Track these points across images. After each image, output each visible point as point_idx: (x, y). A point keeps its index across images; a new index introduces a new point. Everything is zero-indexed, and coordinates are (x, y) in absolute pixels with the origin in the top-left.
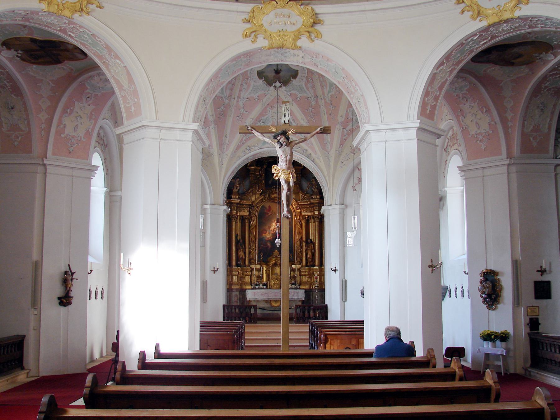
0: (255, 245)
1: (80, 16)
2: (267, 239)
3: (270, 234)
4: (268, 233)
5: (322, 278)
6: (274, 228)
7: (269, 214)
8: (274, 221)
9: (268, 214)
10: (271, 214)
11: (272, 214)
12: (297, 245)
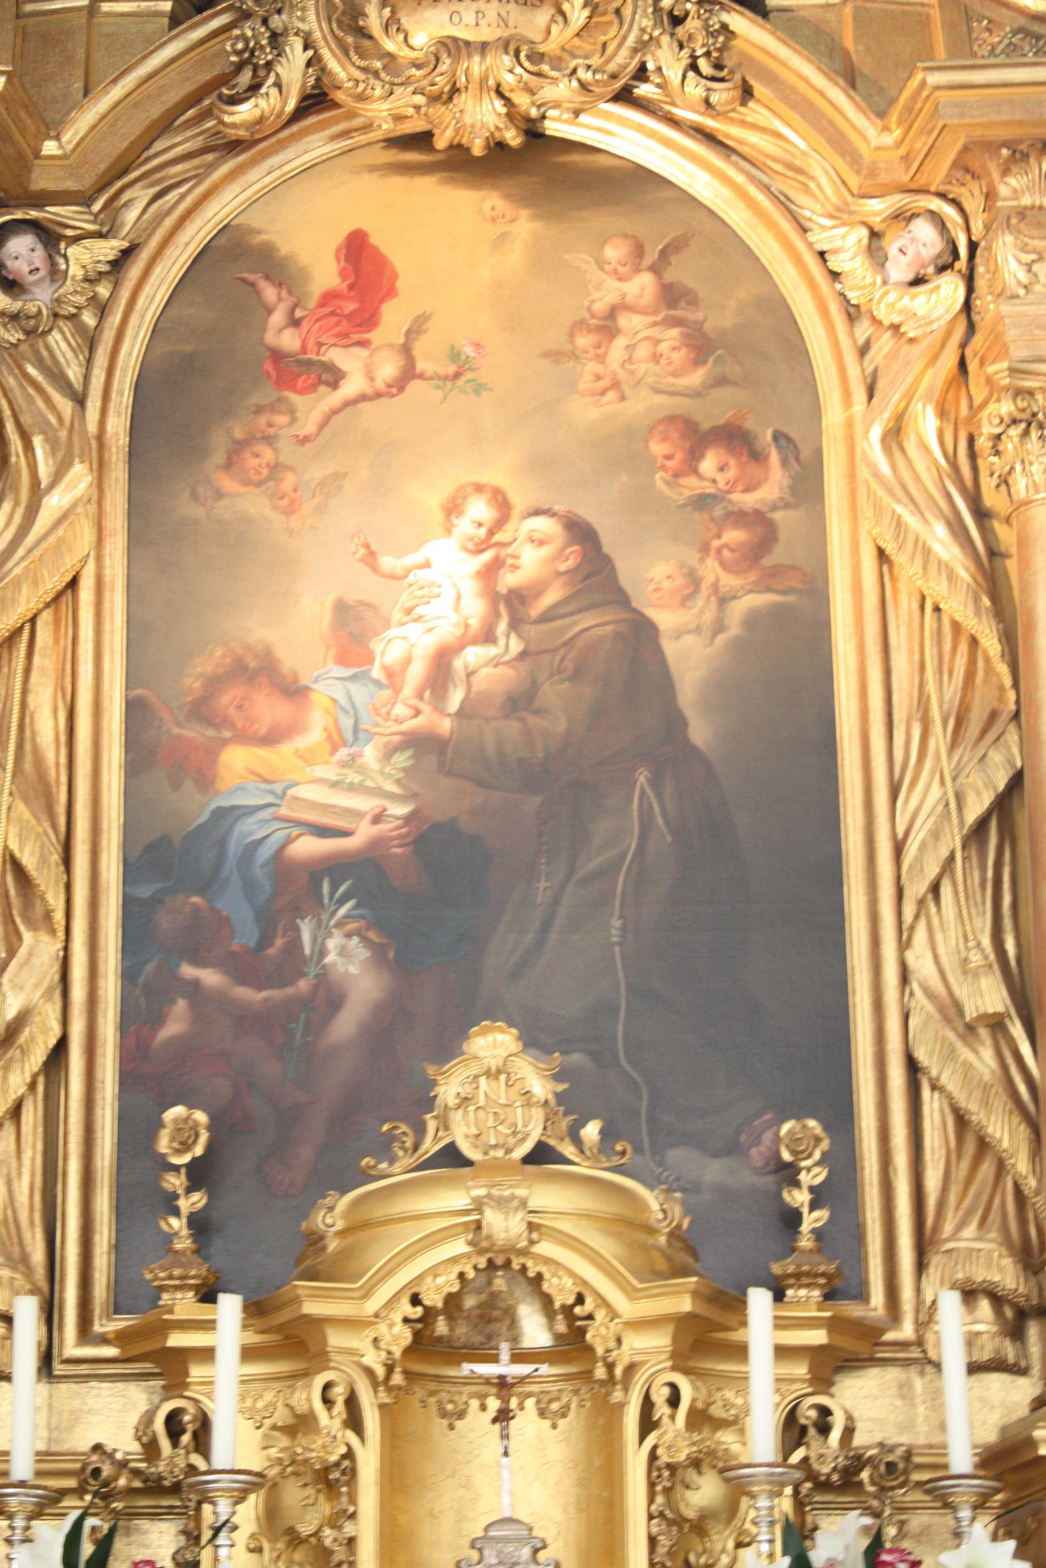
0: (49, 948)
1: (458, 1094)
2: (307, 847)
3: (370, 754)
4: (314, 736)
5: (313, 805)
6: (446, 631)
7: (350, 387)
8: (453, 508)
9: (334, 377)
10: (388, 369)
11: (408, 374)
12: (921, 961)
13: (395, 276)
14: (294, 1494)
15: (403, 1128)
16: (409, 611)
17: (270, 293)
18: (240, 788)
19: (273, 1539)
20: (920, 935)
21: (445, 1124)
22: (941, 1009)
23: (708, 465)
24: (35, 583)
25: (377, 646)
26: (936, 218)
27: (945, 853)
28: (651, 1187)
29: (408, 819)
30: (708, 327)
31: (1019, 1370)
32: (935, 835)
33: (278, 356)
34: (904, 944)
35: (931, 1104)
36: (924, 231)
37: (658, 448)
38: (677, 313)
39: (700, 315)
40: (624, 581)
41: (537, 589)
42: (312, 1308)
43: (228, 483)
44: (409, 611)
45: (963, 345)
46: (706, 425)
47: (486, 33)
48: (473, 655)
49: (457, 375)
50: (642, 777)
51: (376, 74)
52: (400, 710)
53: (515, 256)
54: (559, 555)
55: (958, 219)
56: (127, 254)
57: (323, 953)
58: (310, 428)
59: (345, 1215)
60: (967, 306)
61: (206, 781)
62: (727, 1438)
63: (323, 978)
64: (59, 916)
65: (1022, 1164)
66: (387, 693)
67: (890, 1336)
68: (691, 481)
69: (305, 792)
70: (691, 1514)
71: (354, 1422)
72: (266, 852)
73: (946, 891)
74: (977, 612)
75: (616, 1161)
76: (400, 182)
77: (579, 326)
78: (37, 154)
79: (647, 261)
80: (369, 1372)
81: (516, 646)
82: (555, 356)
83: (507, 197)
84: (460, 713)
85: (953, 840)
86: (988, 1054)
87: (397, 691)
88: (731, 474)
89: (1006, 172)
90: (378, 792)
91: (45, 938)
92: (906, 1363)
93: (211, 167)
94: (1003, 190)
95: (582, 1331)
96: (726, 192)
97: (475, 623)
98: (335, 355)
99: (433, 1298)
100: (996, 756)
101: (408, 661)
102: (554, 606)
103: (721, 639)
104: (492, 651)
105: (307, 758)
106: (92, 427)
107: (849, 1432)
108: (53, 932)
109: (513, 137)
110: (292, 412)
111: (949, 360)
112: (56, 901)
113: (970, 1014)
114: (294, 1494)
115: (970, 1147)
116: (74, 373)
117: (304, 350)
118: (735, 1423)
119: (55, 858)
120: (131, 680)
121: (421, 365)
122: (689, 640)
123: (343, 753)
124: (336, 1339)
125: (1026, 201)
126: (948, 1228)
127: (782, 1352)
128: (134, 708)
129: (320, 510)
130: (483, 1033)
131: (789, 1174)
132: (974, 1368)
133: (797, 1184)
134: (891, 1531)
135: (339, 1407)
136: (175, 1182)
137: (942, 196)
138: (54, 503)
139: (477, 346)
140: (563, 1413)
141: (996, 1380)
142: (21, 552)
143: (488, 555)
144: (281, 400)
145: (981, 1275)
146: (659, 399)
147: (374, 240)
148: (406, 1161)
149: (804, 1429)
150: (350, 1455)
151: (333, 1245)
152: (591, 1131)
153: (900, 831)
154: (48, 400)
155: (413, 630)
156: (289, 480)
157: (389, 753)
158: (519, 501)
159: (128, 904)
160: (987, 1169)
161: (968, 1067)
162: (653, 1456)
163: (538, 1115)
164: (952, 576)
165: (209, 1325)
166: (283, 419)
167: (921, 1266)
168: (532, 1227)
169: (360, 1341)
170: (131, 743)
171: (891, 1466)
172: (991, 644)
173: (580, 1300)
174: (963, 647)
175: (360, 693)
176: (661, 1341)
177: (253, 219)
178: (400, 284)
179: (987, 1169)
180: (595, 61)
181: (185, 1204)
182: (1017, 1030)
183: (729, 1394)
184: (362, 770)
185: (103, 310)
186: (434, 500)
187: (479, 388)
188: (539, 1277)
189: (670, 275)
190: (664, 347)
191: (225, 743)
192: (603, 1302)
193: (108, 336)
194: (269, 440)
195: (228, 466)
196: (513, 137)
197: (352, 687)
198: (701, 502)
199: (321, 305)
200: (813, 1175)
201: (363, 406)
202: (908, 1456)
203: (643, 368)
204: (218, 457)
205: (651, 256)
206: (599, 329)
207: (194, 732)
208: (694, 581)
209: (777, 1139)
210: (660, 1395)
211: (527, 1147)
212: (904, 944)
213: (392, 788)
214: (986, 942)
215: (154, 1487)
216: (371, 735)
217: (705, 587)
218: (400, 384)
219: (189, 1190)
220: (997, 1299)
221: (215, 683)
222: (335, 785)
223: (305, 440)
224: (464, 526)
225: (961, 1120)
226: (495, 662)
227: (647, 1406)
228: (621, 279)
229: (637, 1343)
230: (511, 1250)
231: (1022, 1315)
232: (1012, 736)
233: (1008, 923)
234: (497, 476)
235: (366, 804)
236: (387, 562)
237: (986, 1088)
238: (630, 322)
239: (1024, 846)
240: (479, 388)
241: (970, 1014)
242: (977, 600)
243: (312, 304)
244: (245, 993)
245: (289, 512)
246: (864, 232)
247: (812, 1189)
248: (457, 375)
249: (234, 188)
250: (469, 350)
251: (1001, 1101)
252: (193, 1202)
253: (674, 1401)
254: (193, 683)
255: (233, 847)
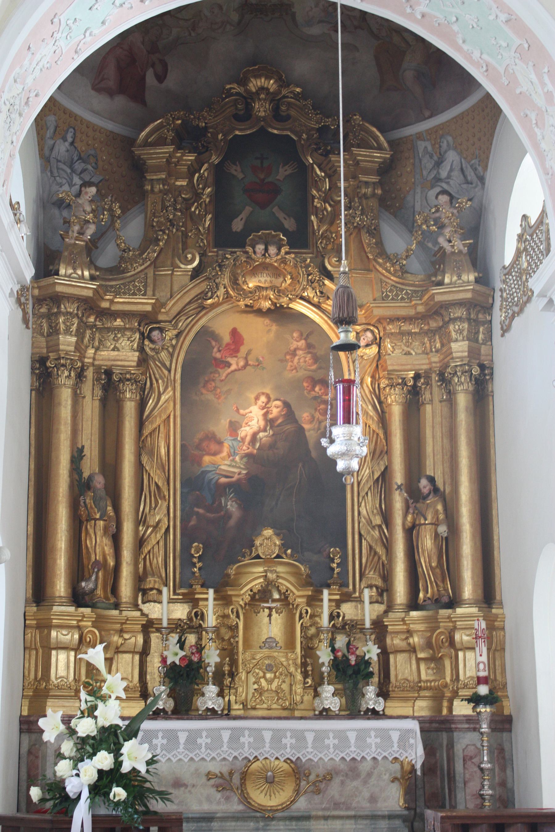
2: (223, 480)
3: (237, 458)
4: (224, 454)
5: (224, 470)
6: (255, 428)
7: (233, 367)
8: (257, 398)
9: (229, 365)
10: (242, 363)
11: (246, 365)
12: (364, 512)
13: (243, 339)
14: (223, 630)
15: (247, 550)
16: (247, 424)
17: (214, 343)
18: (208, 466)
19: (219, 640)
20: (363, 504)
21: (256, 549)
22: (367, 522)
23: (317, 389)
24: (160, 417)
25: (239, 432)
26: (372, 332)
27: (369, 486)
28: (302, 564)
29: (246, 474)
30: (318, 354)
31: (382, 603)
32: (367, 481)
33: (215, 359)
34: (359, 506)
35: (364, 543)
36: (369, 334)
37: (305, 384)
38: (311, 350)
39: (316, 351)
40: (297, 417)
41: (276, 419)
42: (230, 593)
43: (204, 391)
44: (247, 424)
45: (378, 361)
46: (317, 379)
47: (267, 285)
48: (261, 434)
49: (258, 365)
50: (300, 465)
51: (241, 295)
52: (244, 448)
53: (272, 335)
54: (282, 411)
55: (377, 331)
56: (179, 333)
57: (227, 506)
58: (223, 378)
59: (235, 570)
60: (379, 352)
61: (200, 464)
62: (317, 619)
63: (227, 511)
64: (167, 497)
65: (384, 558)
66: (241, 444)
67: (353, 596)
68: (313, 393)
69: (223, 467)
70: (309, 636)
71: (238, 616)
72: (214, 481)
73: (369, 494)
74: (378, 428)
75: (294, 558)
76: (244, 315)
77: (287, 353)
78: (160, 311)
79: (303, 337)
80: (241, 606)
81: (271, 433)
82: (281, 361)
83: (270, 320)
84: (259, 449)
85: (371, 483)
86: (377, 532)
87: (244, 443)
88: (322, 391)
89: (388, 324)
90: (239, 467)
91: (164, 502)
92: (357, 601)
93: (200, 312)
94: (388, 328)
95: (287, 597)
96: (323, 321)
97: (262, 427)
98: (229, 359)
99: (255, 590)
100: (382, 463)
101: (246, 436)
102: (281, 423)
103: (319, 432)
104: (266, 434)
105: (223, 459)
106: (172, 378)
107: (344, 617)
108: (165, 500)
109: (273, 308)
110: (219, 373)
111: (374, 365)
112: (166, 493)
113: (374, 524)
114: (223, 630)
115: (373, 554)
116: (168, 364)
117: (222, 358)
118: (319, 616)
119: (166, 483)
120: (182, 439)
121: (250, 362)
122: (312, 432)
123: (231, 458)
124: (234, 599)
125: (393, 331)
126: (367, 572)
127: (330, 600)
128: (182, 446)
129: (225, 398)
130: (266, 530)
131: (332, 560)
132: (371, 603)
133: (334, 562)
134: (352, 639)
135: (235, 613)
136: (195, 560)
137: (374, 326)
138: (163, 398)
139: (263, 358)
140: (281, 612)
141: (376, 605)
142: (157, 409)
143: (265, 410)
144: (217, 370)
145: (374, 583)
146: (306, 372)
147: (239, 330)
148: (248, 558)
149: (334, 617)
150: (237, 623)
151: (232, 577)
152: (289, 551)
153: (359, 479)
154: (162, 371)
155: (247, 428)
156: (219, 391)
157: (241, 458)
158: (272, 397)
159: (182, 493)
160: (376, 558)
161: (373, 535)
162: (302, 624)
163: (277, 548)
164: (373, 419)
165: (207, 593)
166: (217, 375)
167: (361, 580)
168: (277, 576)
169: (239, 599)
170: (182, 455)
171: (353, 625)
172: (382, 435)
173: (287, 591)
174: (375, 436)
175: (235, 443)
176: (304, 600)
177: (210, 325)
178: (245, 342)
179: (376, 558)
180: (293, 293)
181: (197, 565)
182: (384, 527)
183: (318, 609)
184: (236, 462)
185: (174, 347)
186: (252, 396)
187: (263, 368)
188: (278, 586)
189: (309, 341)
190: (307, 359)
191: (204, 455)
192: (292, 591)
193: (176, 355)
194: (213, 380)
195: (204, 387)
196: (273, 308)
197: (233, 442)
198: (315, 398)
199: (226, 346)
200: (337, 560)
201: (236, 372)
202: (356, 623)
203: (302, 364)
204: (202, 385)
205: (305, 336)
206: (292, 354)
207: (196, 452)
208: (313, 417)
209: (330, 552)
210: (304, 612)
211: (275, 555)
212: (359, 506)
213: (242, 466)
214: (378, 506)
215: (190, 627)
216: (238, 454)
217: (316, 419)
218: (245, 367)
219: (198, 562)
220: (377, 588)
221: (201, 441)
222: (229, 466)
223: (222, 380)
224: (260, 403)
225: (371, 547)
226: (266, 436)
227: (301, 614)
228: (297, 341)
229: (299, 600)
230: (273, 581)
231: (383, 591)
232: (386, 458)
233: (383, 502)
234: (267, 391)
235: (236, 470)
236: (242, 411)
237: (376, 541)
238: (300, 353)
239: (387, 484)
240: (263, 368)
241: (374, 524)
242: (378, 425)
243: (224, 346)
244: (209, 515)
245: (218, 398)
246: (355, 333)
247: (337, 564)
248: (258, 365)
249: (205, 317)
250: (261, 359)
251: (379, 543)
252: (199, 565)
253: (307, 612)
254: (196, 440)
255: (206, 480)
